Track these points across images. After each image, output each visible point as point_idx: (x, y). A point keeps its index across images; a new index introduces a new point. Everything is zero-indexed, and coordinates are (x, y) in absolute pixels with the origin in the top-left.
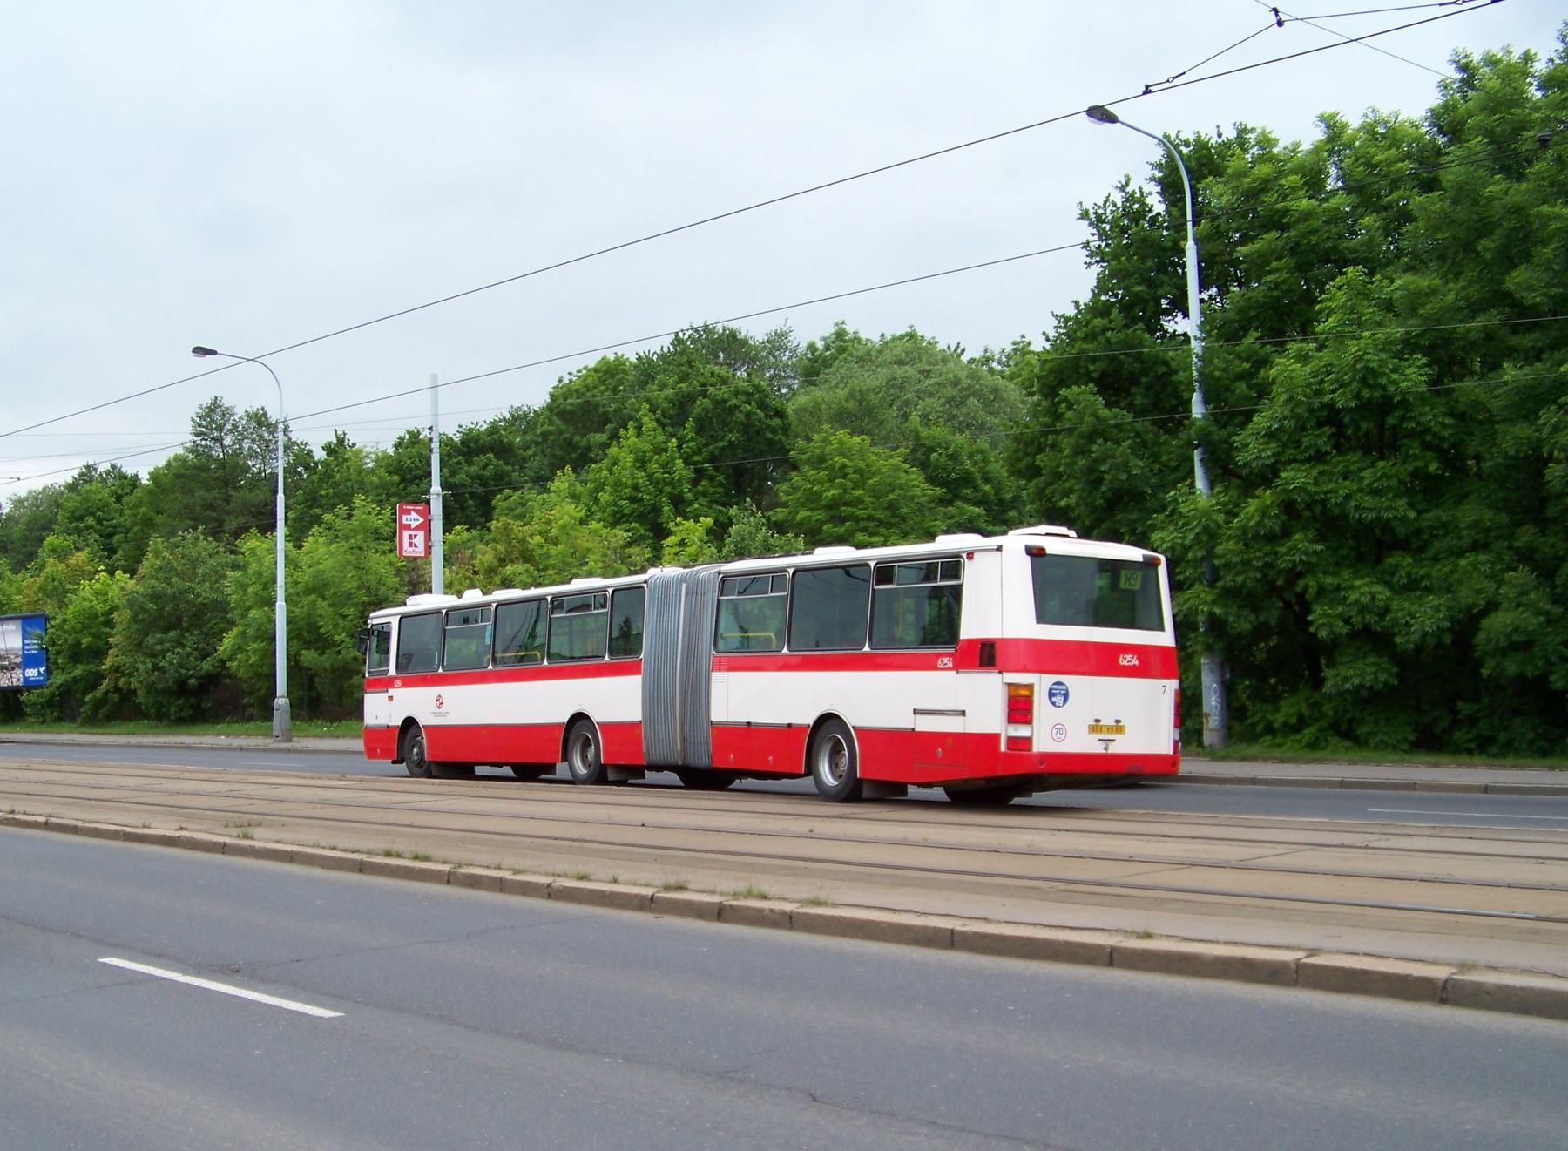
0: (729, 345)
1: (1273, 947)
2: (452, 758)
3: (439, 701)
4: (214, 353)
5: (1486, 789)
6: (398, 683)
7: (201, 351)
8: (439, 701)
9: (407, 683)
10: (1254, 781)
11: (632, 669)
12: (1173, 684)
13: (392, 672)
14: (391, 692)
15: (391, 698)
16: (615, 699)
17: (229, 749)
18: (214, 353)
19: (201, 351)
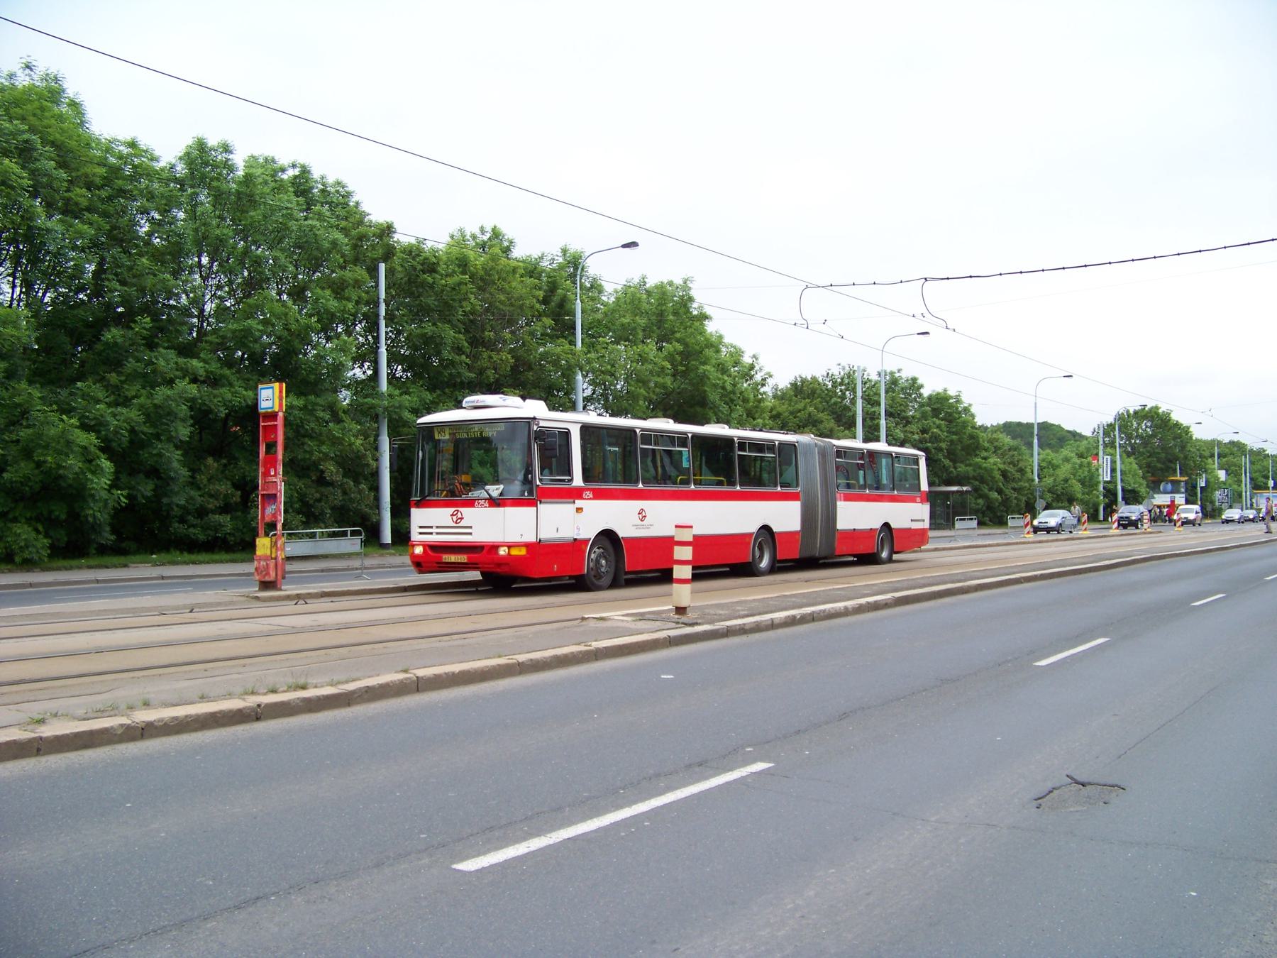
0: (803, 381)
1: (1177, 555)
2: (501, 576)
3: (642, 514)
4: (624, 246)
5: (322, 571)
6: (588, 494)
7: (633, 245)
8: (642, 514)
9: (599, 495)
10: (31, 585)
11: (794, 497)
12: (413, 510)
13: (578, 481)
14: (579, 503)
15: (579, 510)
16: (784, 516)
17: (1047, 541)
18: (624, 246)
19: (633, 245)
